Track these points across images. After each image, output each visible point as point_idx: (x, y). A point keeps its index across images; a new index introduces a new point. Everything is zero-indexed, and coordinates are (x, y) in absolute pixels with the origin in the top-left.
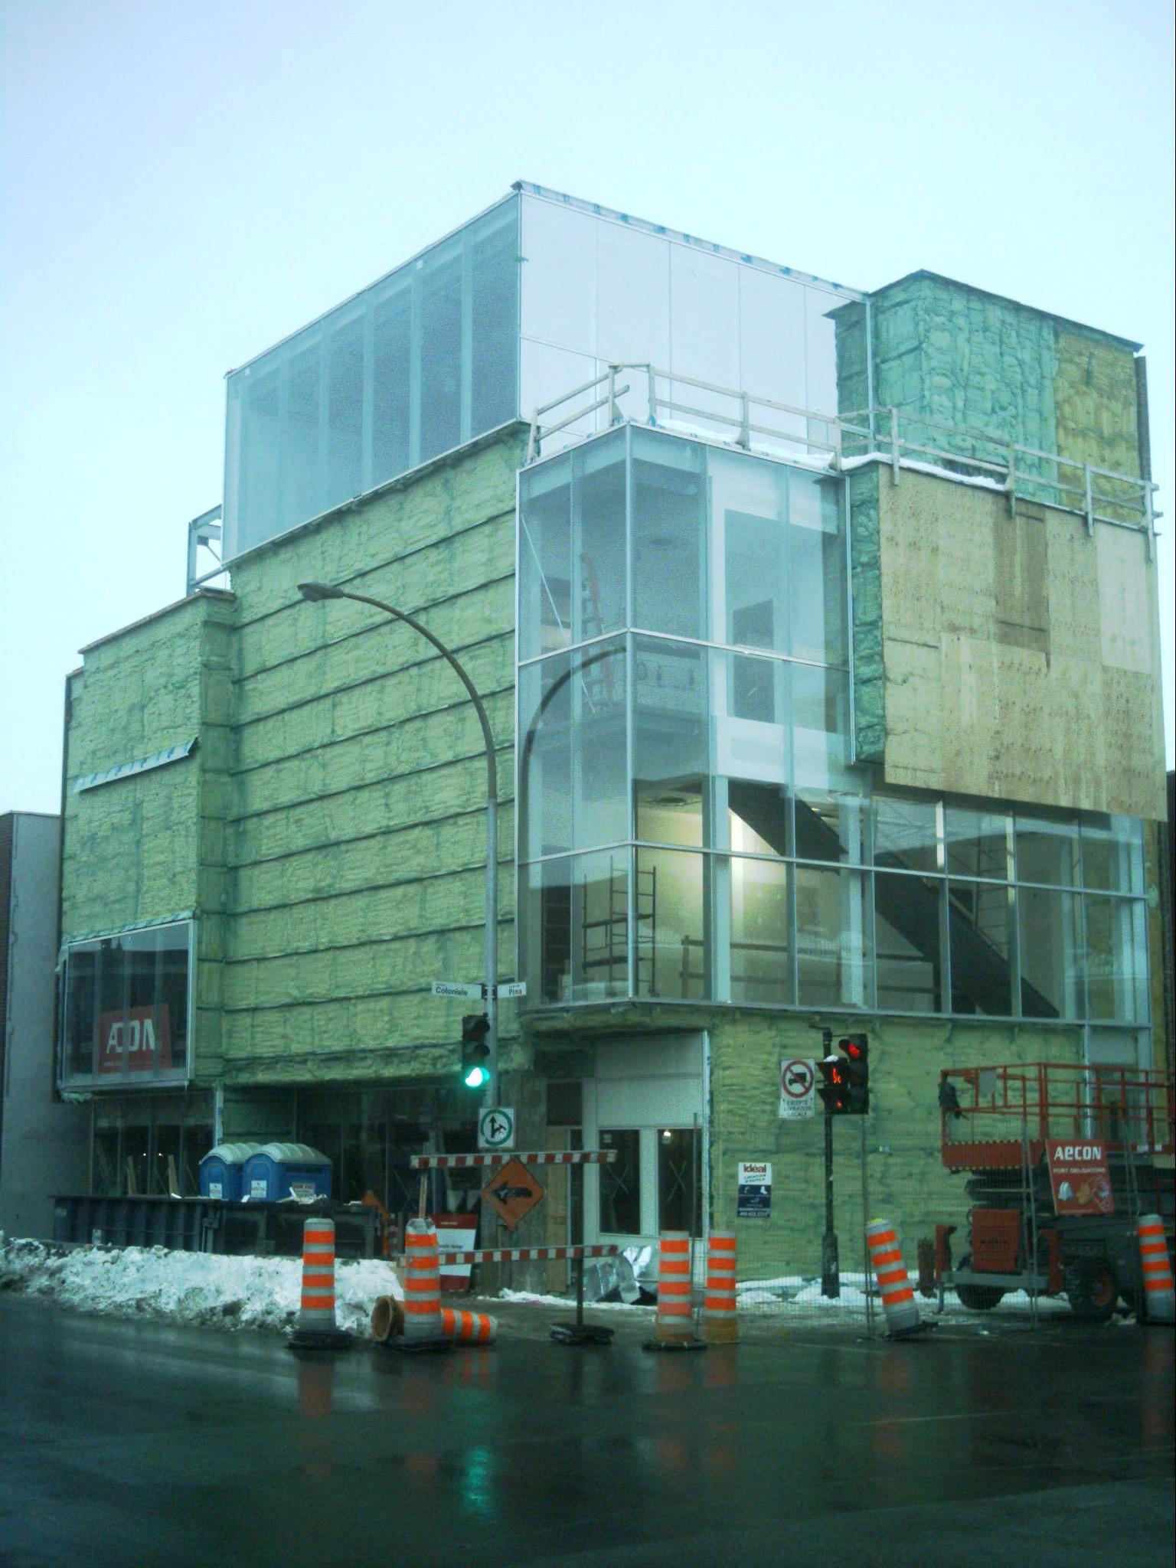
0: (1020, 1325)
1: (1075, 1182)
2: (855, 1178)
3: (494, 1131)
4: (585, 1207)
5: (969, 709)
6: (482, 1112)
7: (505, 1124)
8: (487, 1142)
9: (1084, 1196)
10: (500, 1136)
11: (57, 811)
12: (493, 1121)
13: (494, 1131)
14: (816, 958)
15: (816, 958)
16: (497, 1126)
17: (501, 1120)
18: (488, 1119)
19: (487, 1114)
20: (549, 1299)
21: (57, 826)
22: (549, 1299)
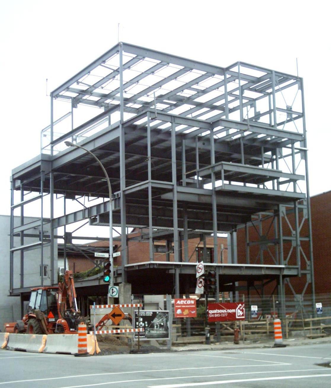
0: (79, 302)
1: (183, 309)
2: (329, 298)
3: (113, 293)
4: (174, 224)
5: (221, 271)
6: (110, 287)
7: (116, 291)
8: (111, 295)
9: (186, 312)
10: (114, 294)
11: (10, 215)
12: (113, 290)
13: (113, 293)
14: (278, 252)
15: (278, 252)
16: (114, 291)
17: (115, 290)
18: (112, 289)
19: (111, 288)
20: (229, 284)
21: (10, 218)
22: (229, 284)
